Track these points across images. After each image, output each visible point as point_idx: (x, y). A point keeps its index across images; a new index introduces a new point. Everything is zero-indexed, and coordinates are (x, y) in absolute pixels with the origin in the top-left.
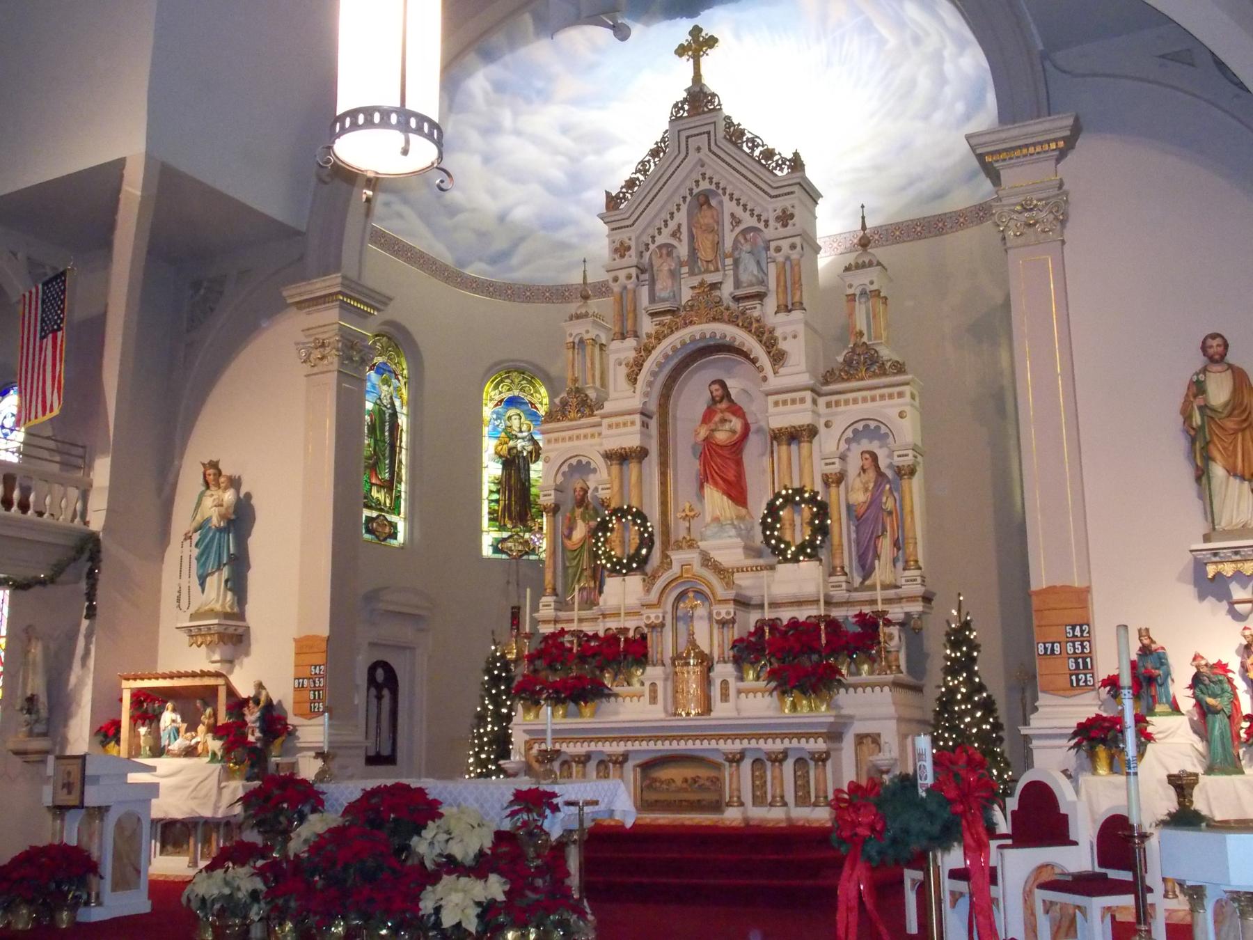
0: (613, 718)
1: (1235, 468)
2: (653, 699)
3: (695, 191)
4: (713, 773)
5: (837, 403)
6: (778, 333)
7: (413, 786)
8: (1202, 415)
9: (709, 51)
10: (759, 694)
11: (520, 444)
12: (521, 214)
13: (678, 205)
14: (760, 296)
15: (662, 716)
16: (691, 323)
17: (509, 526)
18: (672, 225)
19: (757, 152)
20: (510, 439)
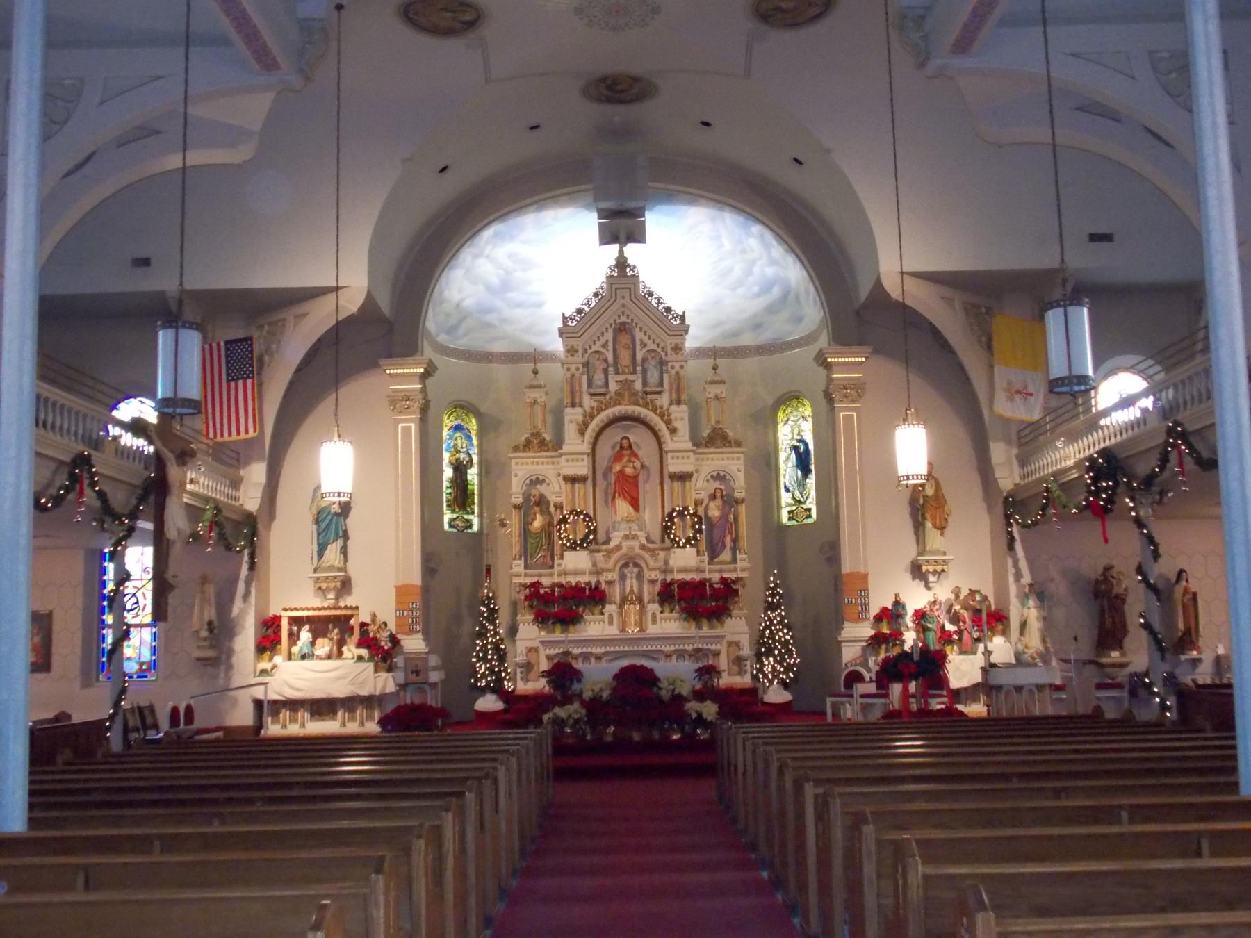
0: (584, 634)
1: (935, 523)
2: (611, 623)
3: (618, 321)
4: (129, 716)
5: (702, 460)
6: (673, 417)
7: (638, 664)
8: (924, 499)
9: (916, 426)
10: (673, 621)
11: (462, 456)
12: (468, 303)
13: (607, 328)
14: (659, 393)
15: (617, 632)
16: (619, 404)
17: (457, 510)
18: (602, 340)
19: (661, 308)
20: (457, 453)
